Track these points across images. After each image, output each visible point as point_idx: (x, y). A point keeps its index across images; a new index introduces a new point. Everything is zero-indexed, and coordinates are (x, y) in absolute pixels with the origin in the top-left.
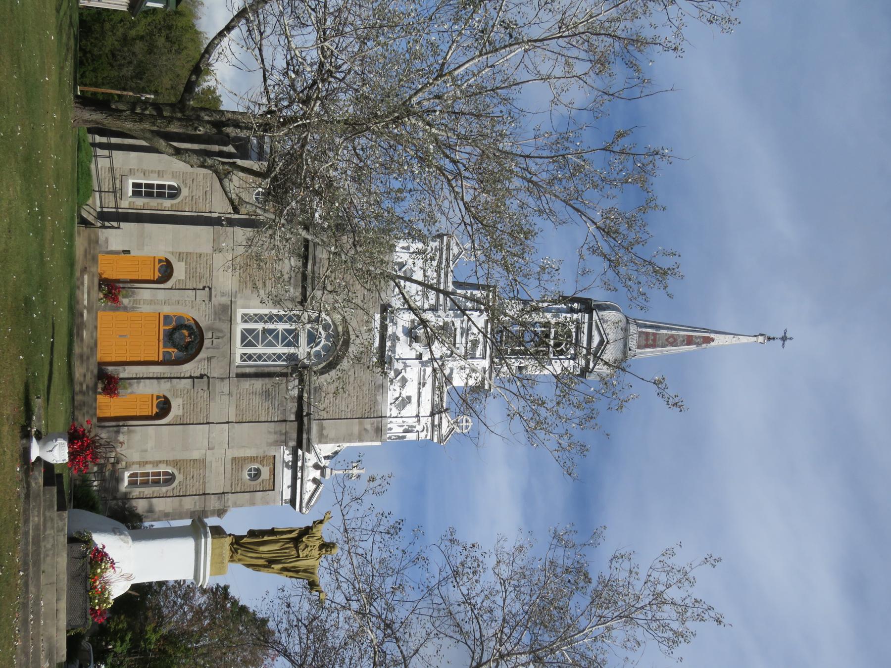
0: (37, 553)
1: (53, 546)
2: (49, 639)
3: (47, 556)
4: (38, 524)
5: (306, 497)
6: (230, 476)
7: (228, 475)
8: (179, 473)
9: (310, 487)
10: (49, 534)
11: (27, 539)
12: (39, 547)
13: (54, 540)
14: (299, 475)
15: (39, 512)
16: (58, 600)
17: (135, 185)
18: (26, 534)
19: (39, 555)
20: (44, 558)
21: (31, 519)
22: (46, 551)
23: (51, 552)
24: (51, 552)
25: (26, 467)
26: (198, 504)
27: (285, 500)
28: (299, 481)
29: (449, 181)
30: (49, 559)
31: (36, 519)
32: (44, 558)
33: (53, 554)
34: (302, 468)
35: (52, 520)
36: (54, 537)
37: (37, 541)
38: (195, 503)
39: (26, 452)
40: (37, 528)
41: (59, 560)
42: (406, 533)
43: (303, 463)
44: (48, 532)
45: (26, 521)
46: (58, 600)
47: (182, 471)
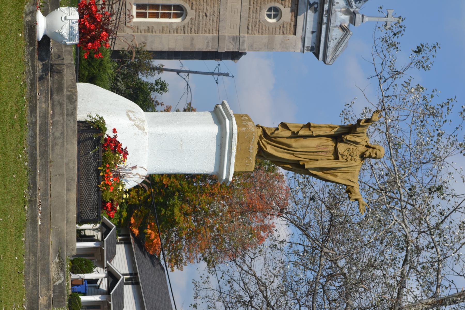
0: (44, 143)
1: (62, 133)
2: (59, 234)
3: (56, 144)
4: (46, 112)
5: (332, 45)
6: (247, 15)
7: (245, 14)
8: (192, 9)
9: (336, 33)
10: (58, 121)
11: (34, 130)
12: (47, 137)
13: (63, 127)
14: (325, 19)
15: (46, 97)
16: (68, 190)
17: (139, 15)
18: (33, 124)
19: (47, 145)
20: (53, 147)
21: (38, 105)
22: (55, 139)
23: (60, 141)
24: (60, 141)
25: (31, 48)
26: (210, 44)
27: (307, 47)
28: (324, 27)
29: (446, 217)
30: (58, 147)
31: (44, 105)
32: (53, 147)
33: (63, 143)
34: (329, 13)
35: (61, 105)
36: (63, 124)
37: (44, 131)
38: (208, 43)
39: (32, 27)
40: (45, 116)
41: (69, 146)
42: (418, 287)
43: (330, 7)
44: (56, 118)
45: (33, 110)
46: (68, 190)
47: (194, 8)
